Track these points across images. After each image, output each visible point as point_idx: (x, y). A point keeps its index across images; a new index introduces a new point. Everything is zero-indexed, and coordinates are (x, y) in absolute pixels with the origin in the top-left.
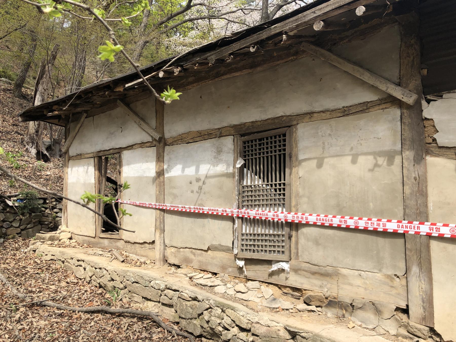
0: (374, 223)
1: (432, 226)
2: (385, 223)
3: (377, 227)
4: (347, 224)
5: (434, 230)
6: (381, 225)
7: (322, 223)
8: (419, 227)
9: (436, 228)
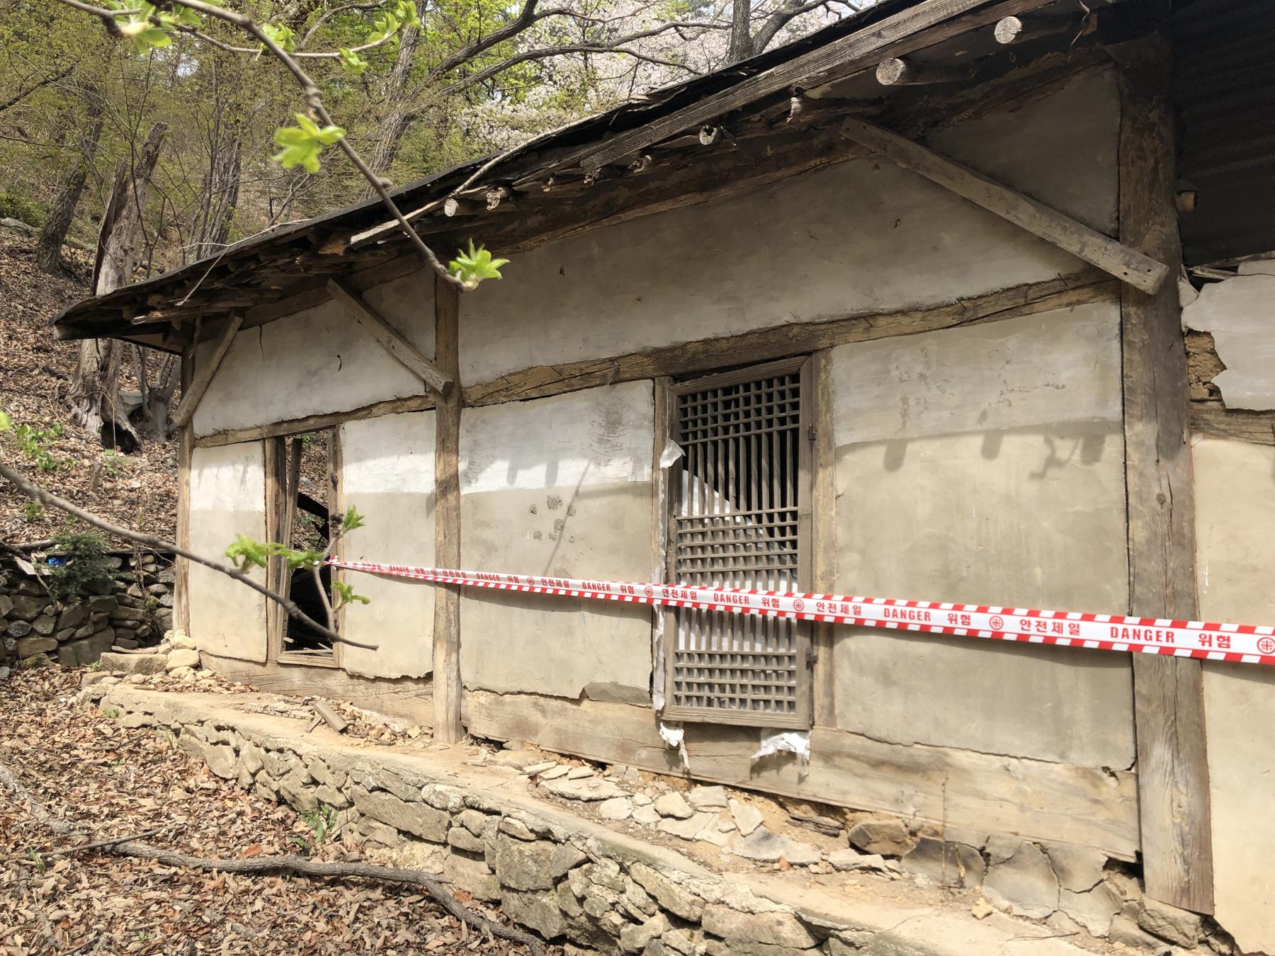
0: (1045, 624)
1: (1207, 633)
2: (1076, 623)
3: (1055, 634)
4: (971, 627)
5: (1215, 642)
6: (1066, 630)
7: (900, 624)
8: (1173, 634)
9: (1219, 638)
